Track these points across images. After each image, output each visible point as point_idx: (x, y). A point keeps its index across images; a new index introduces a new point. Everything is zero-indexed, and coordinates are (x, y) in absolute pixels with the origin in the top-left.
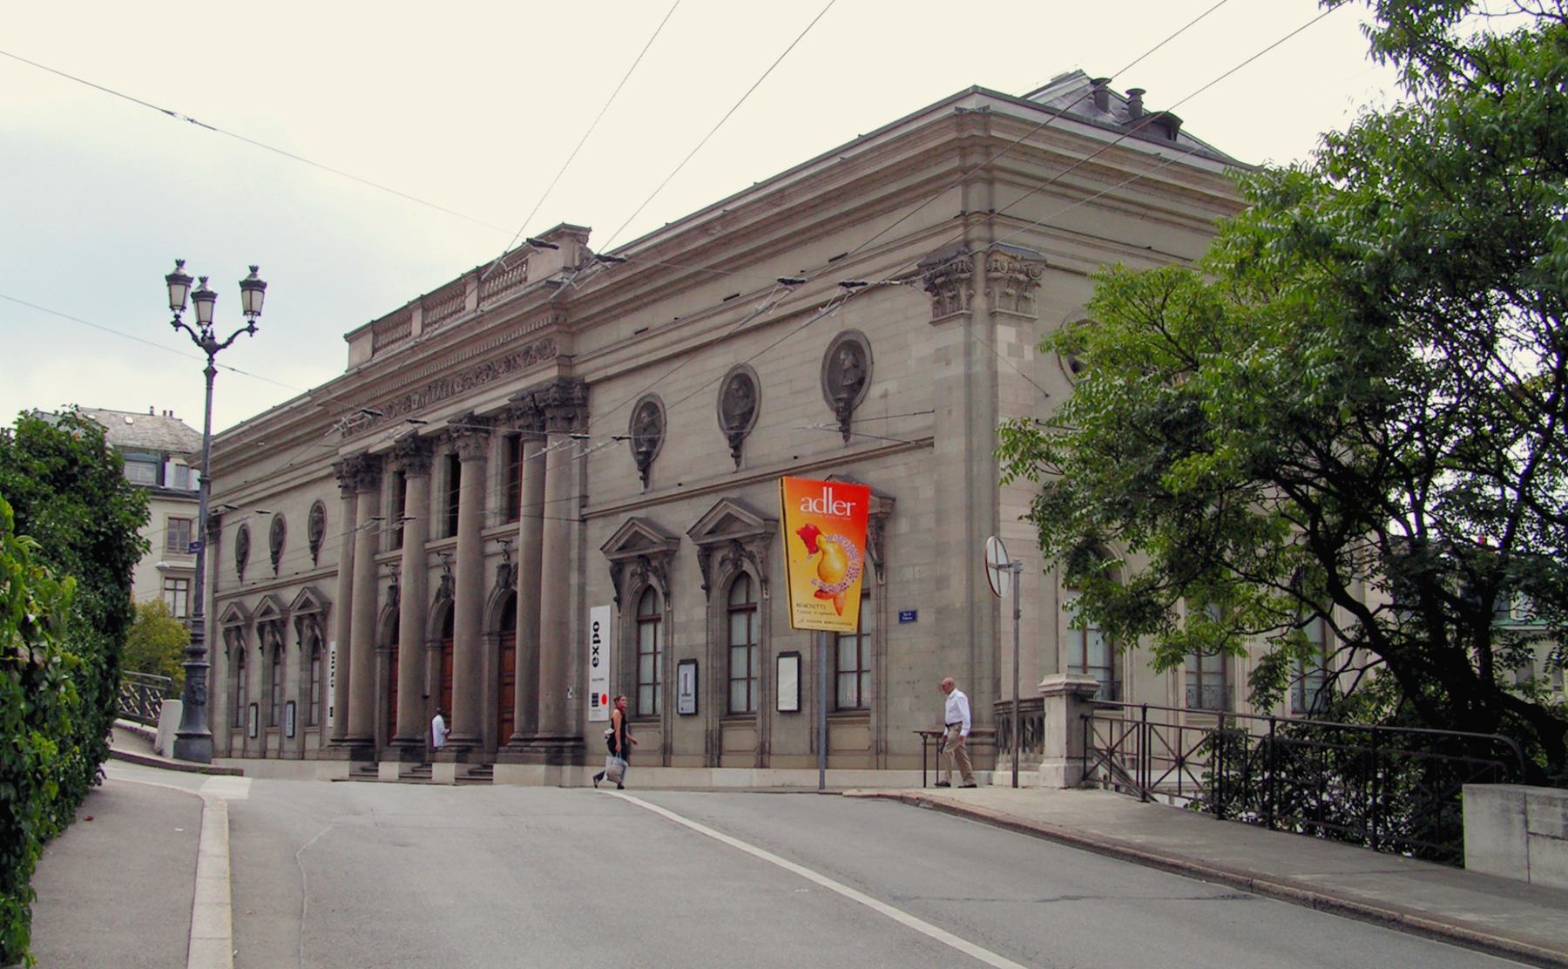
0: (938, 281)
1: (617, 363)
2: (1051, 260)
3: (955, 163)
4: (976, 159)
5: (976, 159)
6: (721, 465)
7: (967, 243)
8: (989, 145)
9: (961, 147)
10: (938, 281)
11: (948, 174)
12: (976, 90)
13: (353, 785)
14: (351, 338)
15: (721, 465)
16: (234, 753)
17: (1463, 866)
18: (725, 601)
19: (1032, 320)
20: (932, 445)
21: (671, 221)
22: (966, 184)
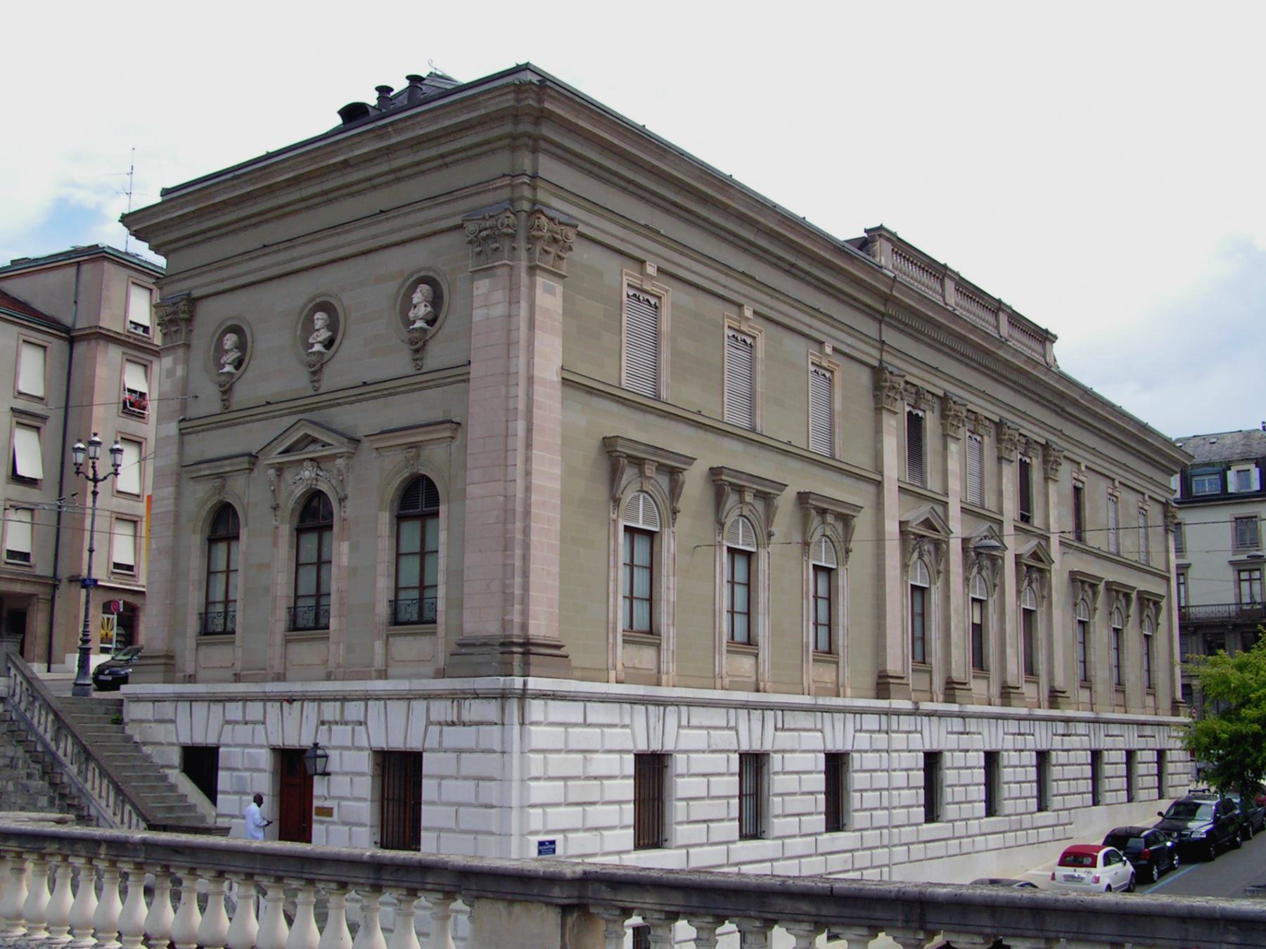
0: (484, 233)
1: (413, 226)
2: (196, 294)
3: (508, 128)
4: (526, 127)
5: (526, 127)
6: (295, 381)
7: (512, 201)
8: (542, 116)
9: (515, 116)
10: (484, 233)
11: (500, 139)
12: (526, 67)
13: (1135, 747)
14: (408, 78)
15: (295, 381)
16: (1185, 666)
17: (275, 750)
18: (1236, 457)
19: (563, 277)
20: (468, 380)
21: (271, 150)
22: (514, 149)
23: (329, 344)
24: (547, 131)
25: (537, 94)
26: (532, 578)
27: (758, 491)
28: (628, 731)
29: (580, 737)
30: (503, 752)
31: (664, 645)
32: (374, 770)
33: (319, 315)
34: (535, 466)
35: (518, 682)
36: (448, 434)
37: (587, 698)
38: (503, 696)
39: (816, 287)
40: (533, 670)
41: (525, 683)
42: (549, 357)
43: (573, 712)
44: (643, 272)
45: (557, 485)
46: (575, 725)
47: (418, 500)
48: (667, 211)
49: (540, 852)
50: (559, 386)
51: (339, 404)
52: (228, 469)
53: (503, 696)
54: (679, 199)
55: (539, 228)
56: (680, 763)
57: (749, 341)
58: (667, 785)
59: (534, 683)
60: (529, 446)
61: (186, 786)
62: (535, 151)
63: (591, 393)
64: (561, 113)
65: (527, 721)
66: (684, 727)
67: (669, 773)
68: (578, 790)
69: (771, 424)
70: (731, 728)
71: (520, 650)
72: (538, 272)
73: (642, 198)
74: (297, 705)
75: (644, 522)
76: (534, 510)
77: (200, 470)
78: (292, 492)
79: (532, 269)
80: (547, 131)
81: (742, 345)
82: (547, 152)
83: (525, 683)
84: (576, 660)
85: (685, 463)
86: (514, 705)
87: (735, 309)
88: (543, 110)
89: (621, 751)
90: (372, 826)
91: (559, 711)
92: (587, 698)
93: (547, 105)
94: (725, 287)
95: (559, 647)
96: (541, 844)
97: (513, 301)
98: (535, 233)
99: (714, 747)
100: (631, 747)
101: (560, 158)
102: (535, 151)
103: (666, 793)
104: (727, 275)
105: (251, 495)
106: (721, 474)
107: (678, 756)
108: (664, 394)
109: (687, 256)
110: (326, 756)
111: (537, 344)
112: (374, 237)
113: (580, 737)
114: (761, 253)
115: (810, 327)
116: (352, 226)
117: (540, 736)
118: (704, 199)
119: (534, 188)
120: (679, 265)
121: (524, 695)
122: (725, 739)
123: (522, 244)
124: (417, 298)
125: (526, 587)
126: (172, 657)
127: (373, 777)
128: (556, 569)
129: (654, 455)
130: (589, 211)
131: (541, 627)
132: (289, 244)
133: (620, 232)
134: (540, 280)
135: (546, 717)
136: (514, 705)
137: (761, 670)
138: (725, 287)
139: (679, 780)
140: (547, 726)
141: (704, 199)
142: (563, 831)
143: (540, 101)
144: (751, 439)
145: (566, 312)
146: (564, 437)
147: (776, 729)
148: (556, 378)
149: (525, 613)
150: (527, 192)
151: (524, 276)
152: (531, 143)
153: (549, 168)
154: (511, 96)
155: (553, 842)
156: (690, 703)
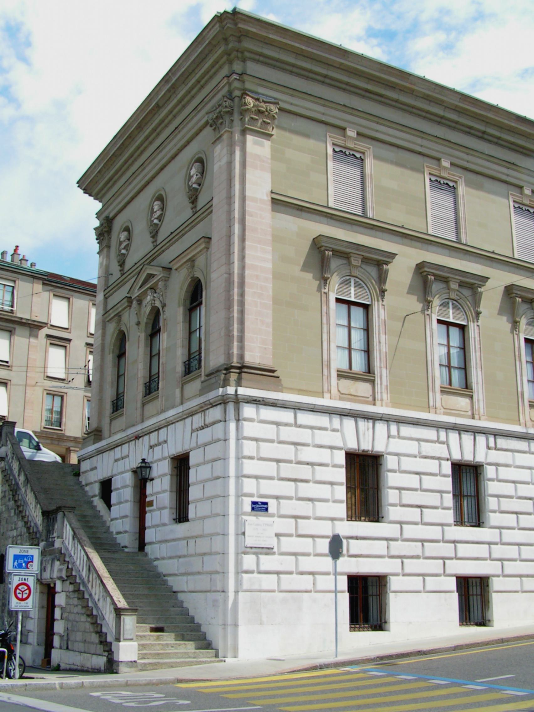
8: (243, 35)
23: (160, 218)
24: (247, 44)
25: (233, 20)
26: (247, 324)
27: (461, 282)
28: (339, 434)
29: (287, 433)
30: (225, 440)
31: (378, 381)
32: (172, 471)
33: (156, 203)
34: (248, 252)
35: (231, 390)
36: (203, 246)
37: (297, 408)
38: (224, 401)
39: (510, 149)
40: (243, 382)
41: (236, 391)
42: (258, 185)
43: (287, 416)
44: (344, 136)
45: (269, 265)
46: (286, 425)
47: (195, 296)
48: (363, 97)
49: (253, 509)
50: (269, 203)
51: (163, 251)
52: (120, 309)
53: (224, 401)
54: (369, 87)
55: (245, 104)
56: (390, 462)
57: (451, 184)
58: (382, 479)
59: (242, 391)
60: (243, 239)
61: (98, 503)
62: (244, 61)
63: (301, 210)
64: (254, 30)
65: (241, 418)
66: (394, 437)
67: (383, 469)
68: (287, 470)
69: (470, 238)
70: (443, 443)
71: (238, 371)
72: (248, 132)
73: (339, 88)
74: (141, 439)
75: (356, 297)
76: (247, 280)
77: (110, 315)
78: (145, 312)
79: (244, 132)
80: (247, 44)
81: (445, 187)
82: (254, 60)
83: (236, 391)
84: (285, 381)
85: (389, 257)
86: (231, 407)
87: (435, 162)
88: (240, 30)
89: (332, 448)
90: (171, 508)
91: (267, 413)
92: (297, 408)
93: (240, 25)
94: (422, 146)
95: (273, 371)
96: (254, 503)
97: (232, 153)
98: (243, 108)
99: (424, 454)
100: (341, 444)
101: (264, 63)
102: (244, 61)
103: (382, 484)
104: (422, 138)
105: (130, 319)
106: (423, 267)
107: (389, 457)
108: (370, 214)
109: (382, 124)
110: (150, 467)
111: (248, 176)
112: (175, 145)
113: (287, 433)
114: (454, 125)
115: (508, 175)
116: (165, 143)
117: (249, 429)
118: (392, 86)
119: (243, 82)
120: (377, 131)
121: (237, 401)
122: (440, 450)
123: (236, 117)
124: (193, 172)
125: (242, 331)
126: (101, 431)
127: (171, 475)
128: (269, 320)
129: (357, 250)
130: (292, 96)
131: (254, 356)
132: (142, 167)
133: (321, 109)
134: (250, 138)
135: (442, 503)
136: (231, 407)
137: (476, 406)
138: (422, 146)
139: (390, 474)
140: (256, 422)
141: (392, 86)
142: (277, 498)
143: (236, 24)
144: (457, 249)
145: (273, 158)
146: (274, 236)
147: (488, 448)
148: (267, 198)
149: (242, 348)
150: (236, 84)
151: (237, 136)
152: (240, 55)
153: (253, 68)
154: (217, 25)
155: (266, 504)
156: (400, 421)
